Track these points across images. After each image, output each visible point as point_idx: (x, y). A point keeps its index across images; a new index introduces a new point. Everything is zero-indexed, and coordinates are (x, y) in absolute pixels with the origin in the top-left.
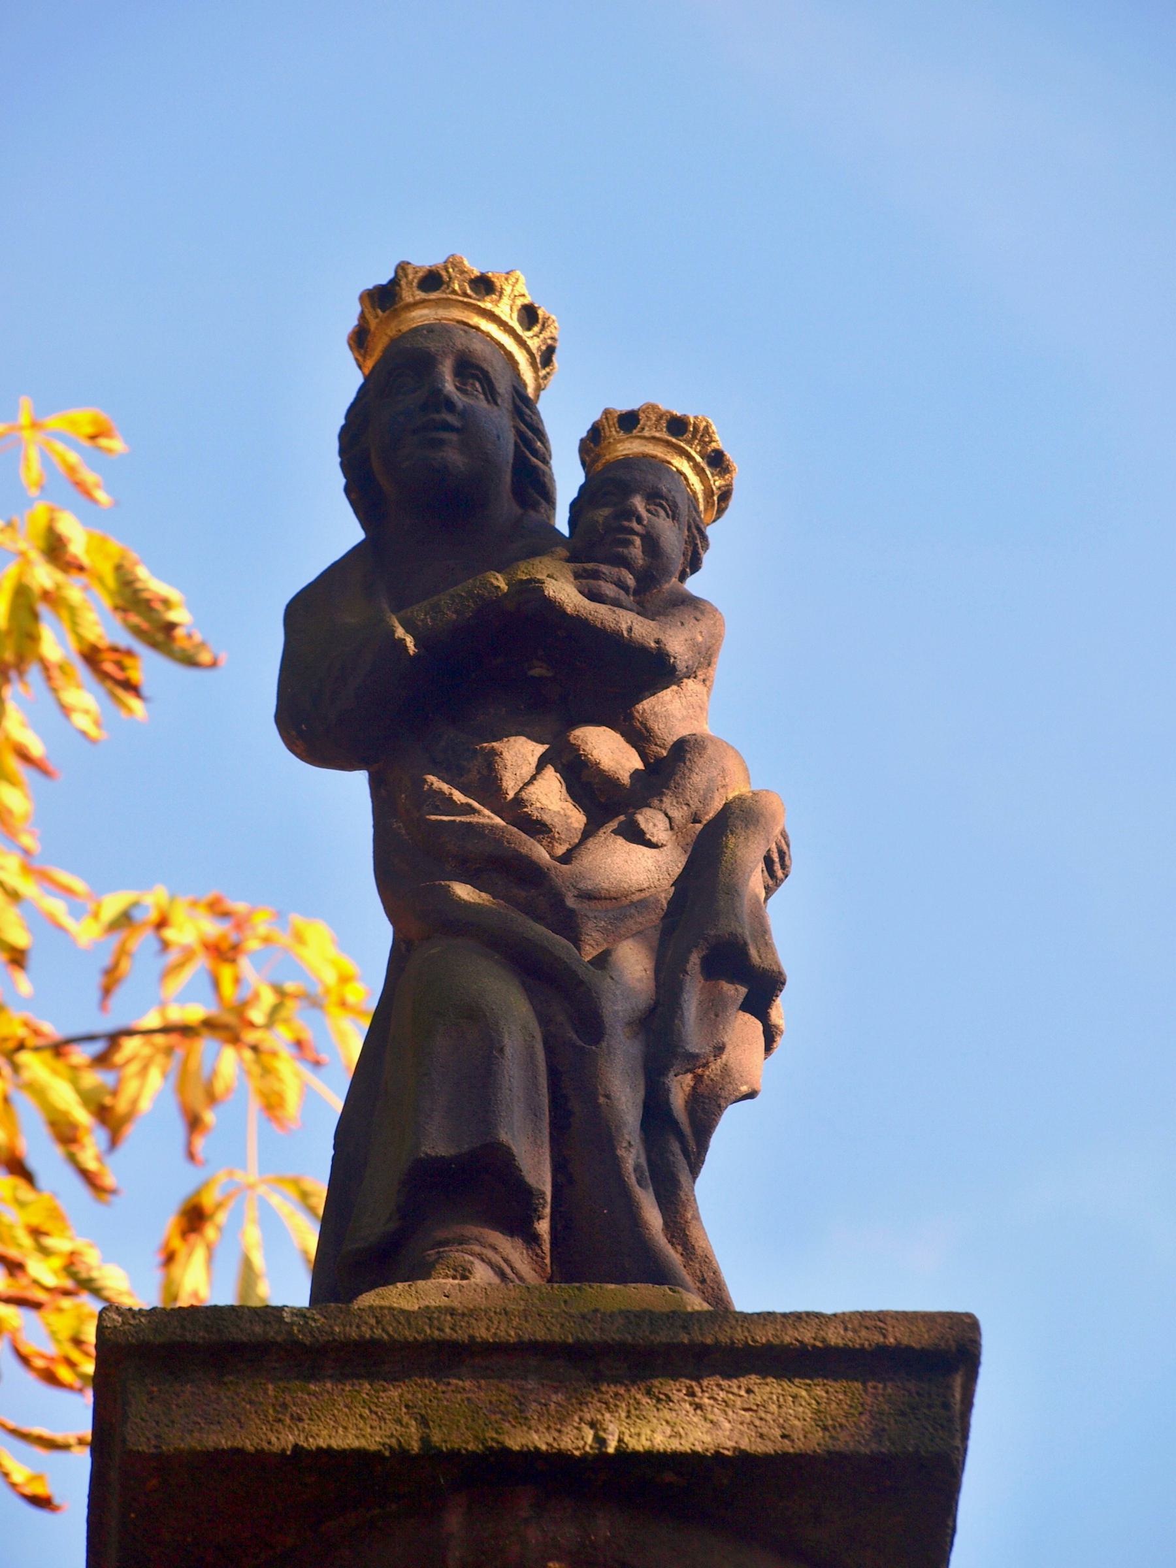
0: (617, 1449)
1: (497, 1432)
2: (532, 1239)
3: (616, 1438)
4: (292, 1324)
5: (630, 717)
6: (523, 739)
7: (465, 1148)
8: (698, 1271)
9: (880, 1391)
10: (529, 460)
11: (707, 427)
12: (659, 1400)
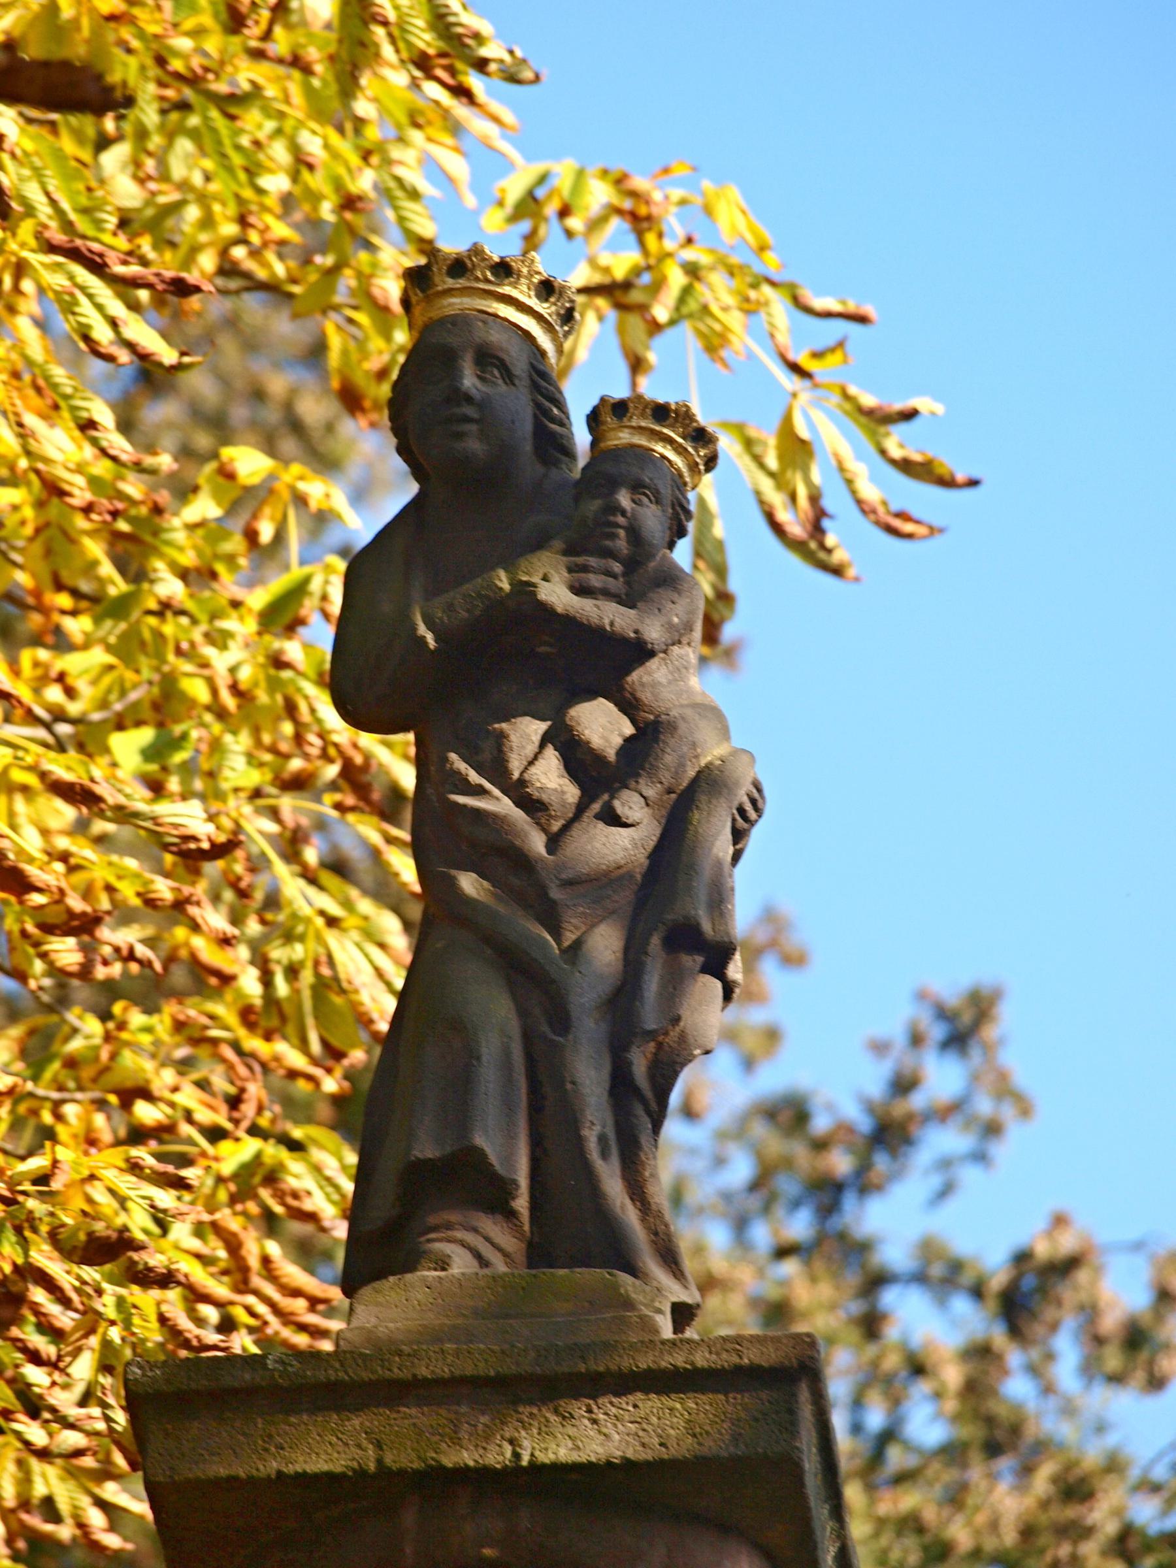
0: (530, 1462)
1: (436, 1453)
3: (529, 1452)
4: (274, 1370)
5: (621, 688)
6: (528, 718)
7: (448, 1150)
8: (652, 1225)
9: (739, 1401)
10: (546, 426)
12: (564, 1418)
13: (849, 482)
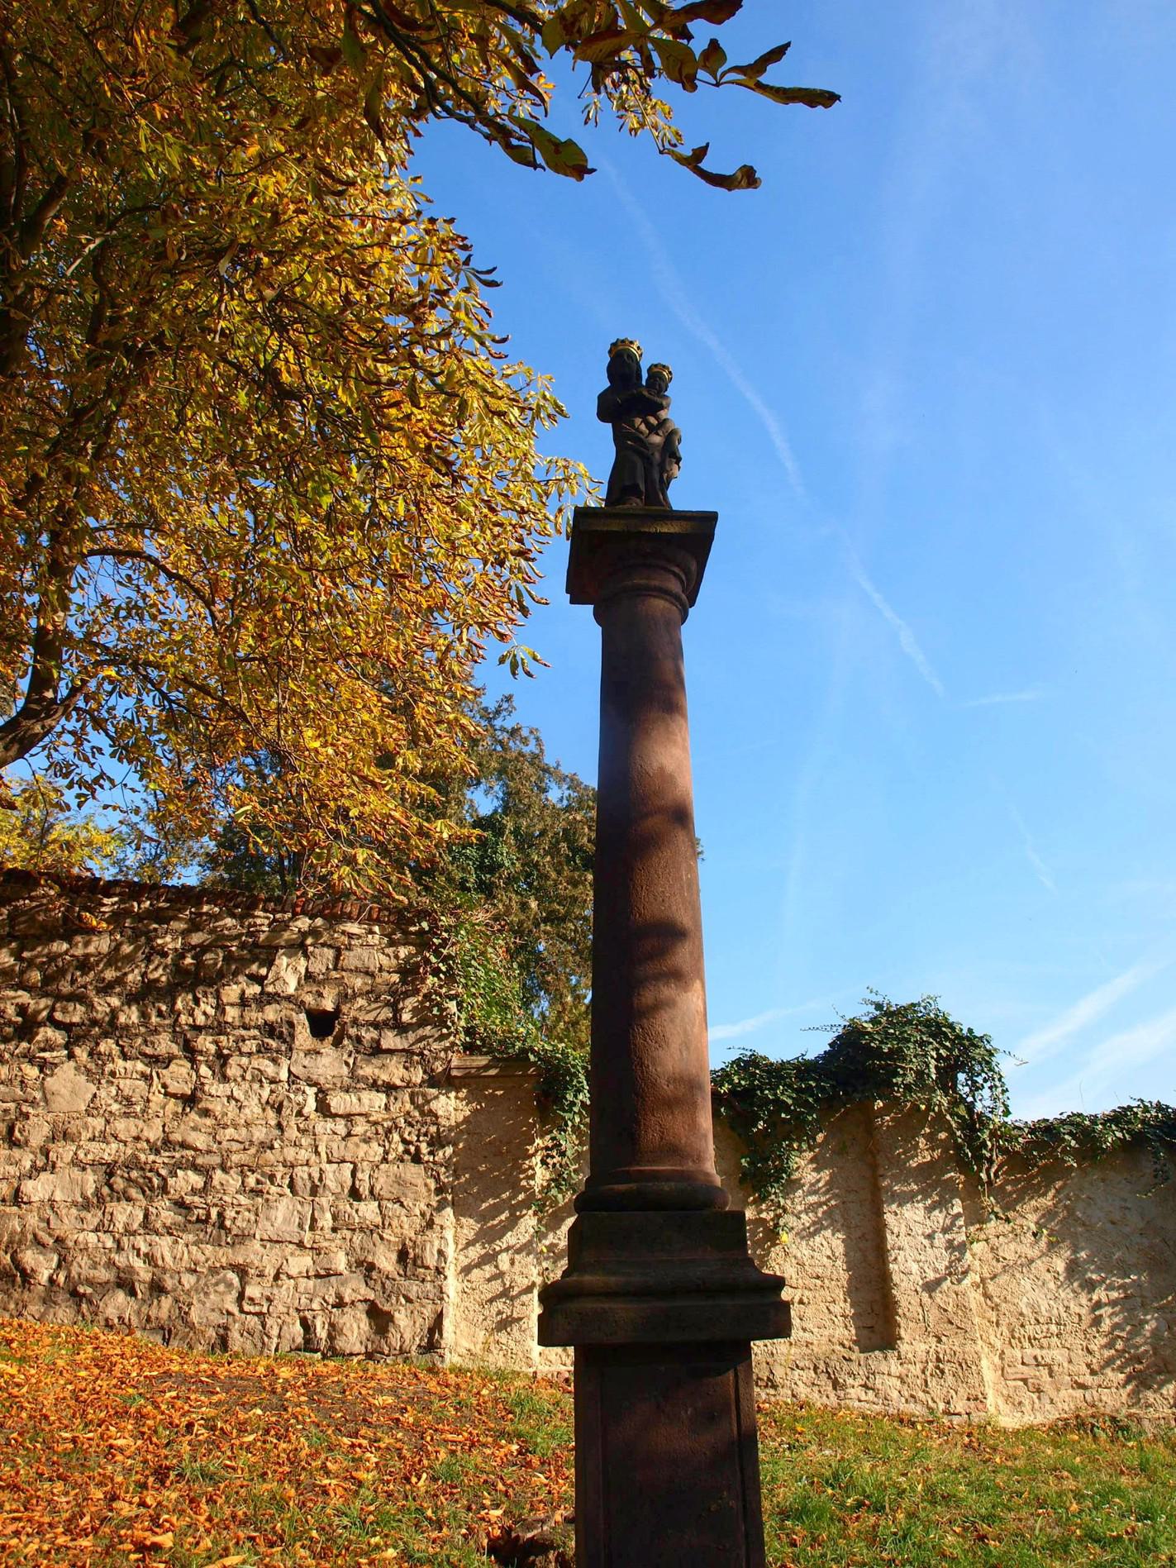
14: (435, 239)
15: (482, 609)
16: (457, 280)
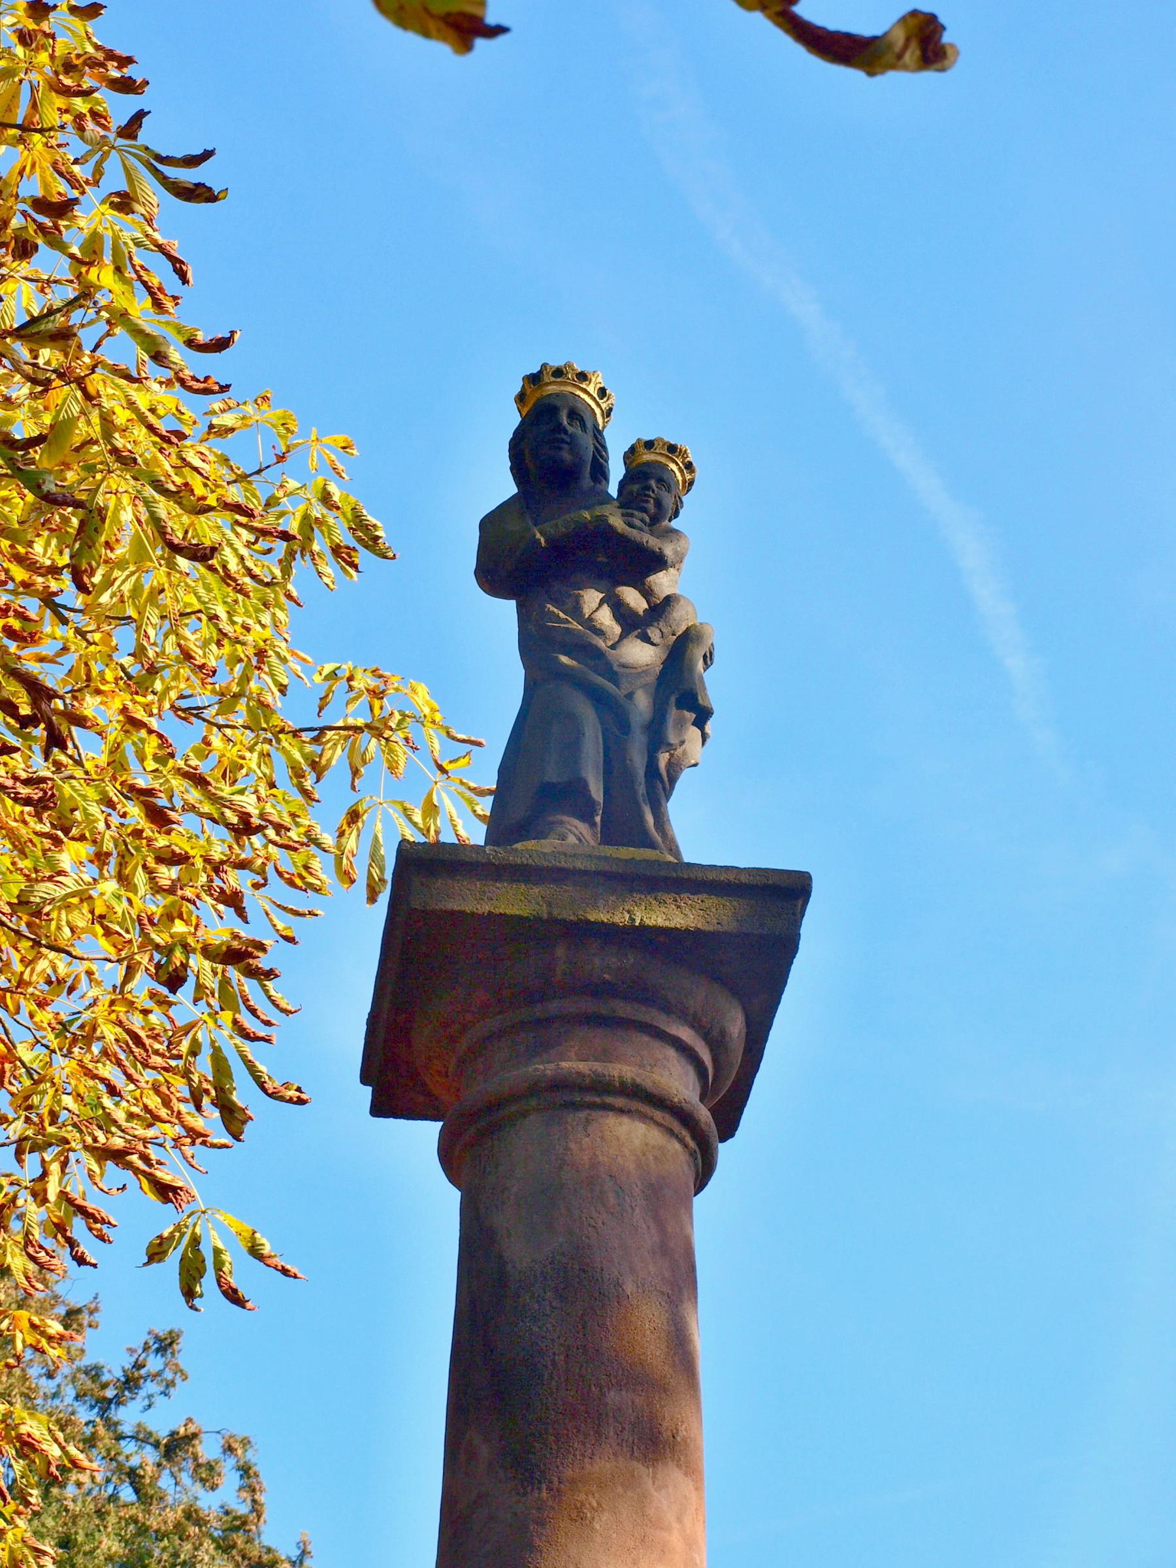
2: (593, 825)
5: (644, 584)
11: (686, 451)
13: (454, 826)
14: (43, 57)
15: (107, 1102)
16: (98, 172)
